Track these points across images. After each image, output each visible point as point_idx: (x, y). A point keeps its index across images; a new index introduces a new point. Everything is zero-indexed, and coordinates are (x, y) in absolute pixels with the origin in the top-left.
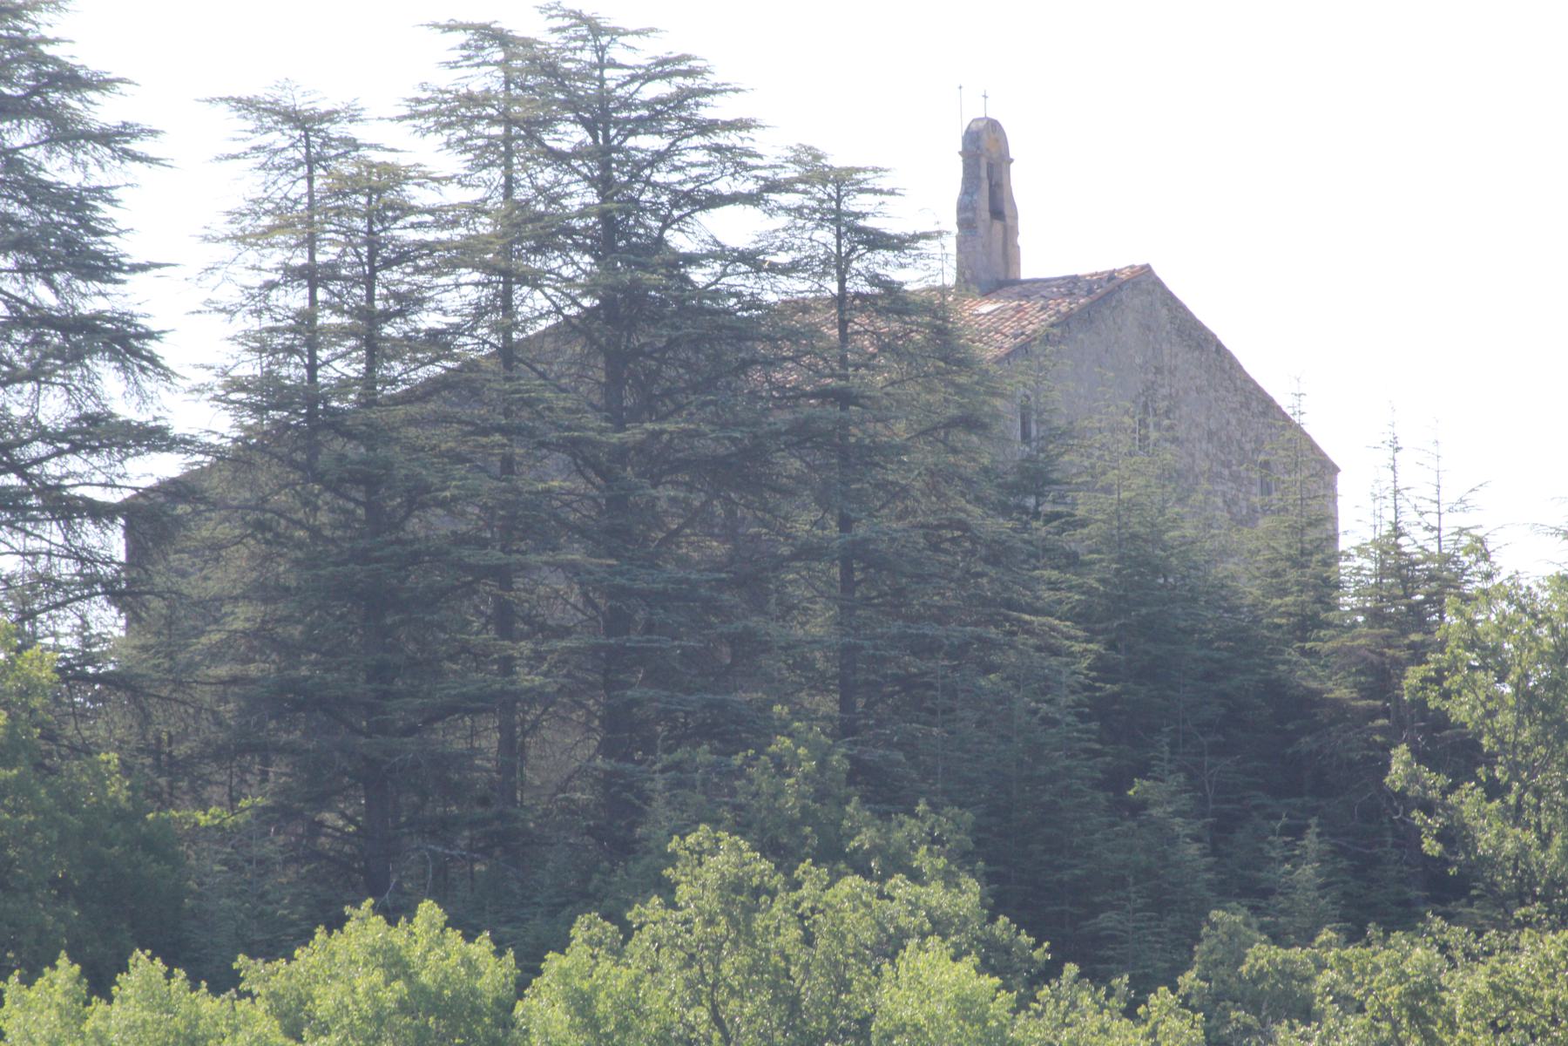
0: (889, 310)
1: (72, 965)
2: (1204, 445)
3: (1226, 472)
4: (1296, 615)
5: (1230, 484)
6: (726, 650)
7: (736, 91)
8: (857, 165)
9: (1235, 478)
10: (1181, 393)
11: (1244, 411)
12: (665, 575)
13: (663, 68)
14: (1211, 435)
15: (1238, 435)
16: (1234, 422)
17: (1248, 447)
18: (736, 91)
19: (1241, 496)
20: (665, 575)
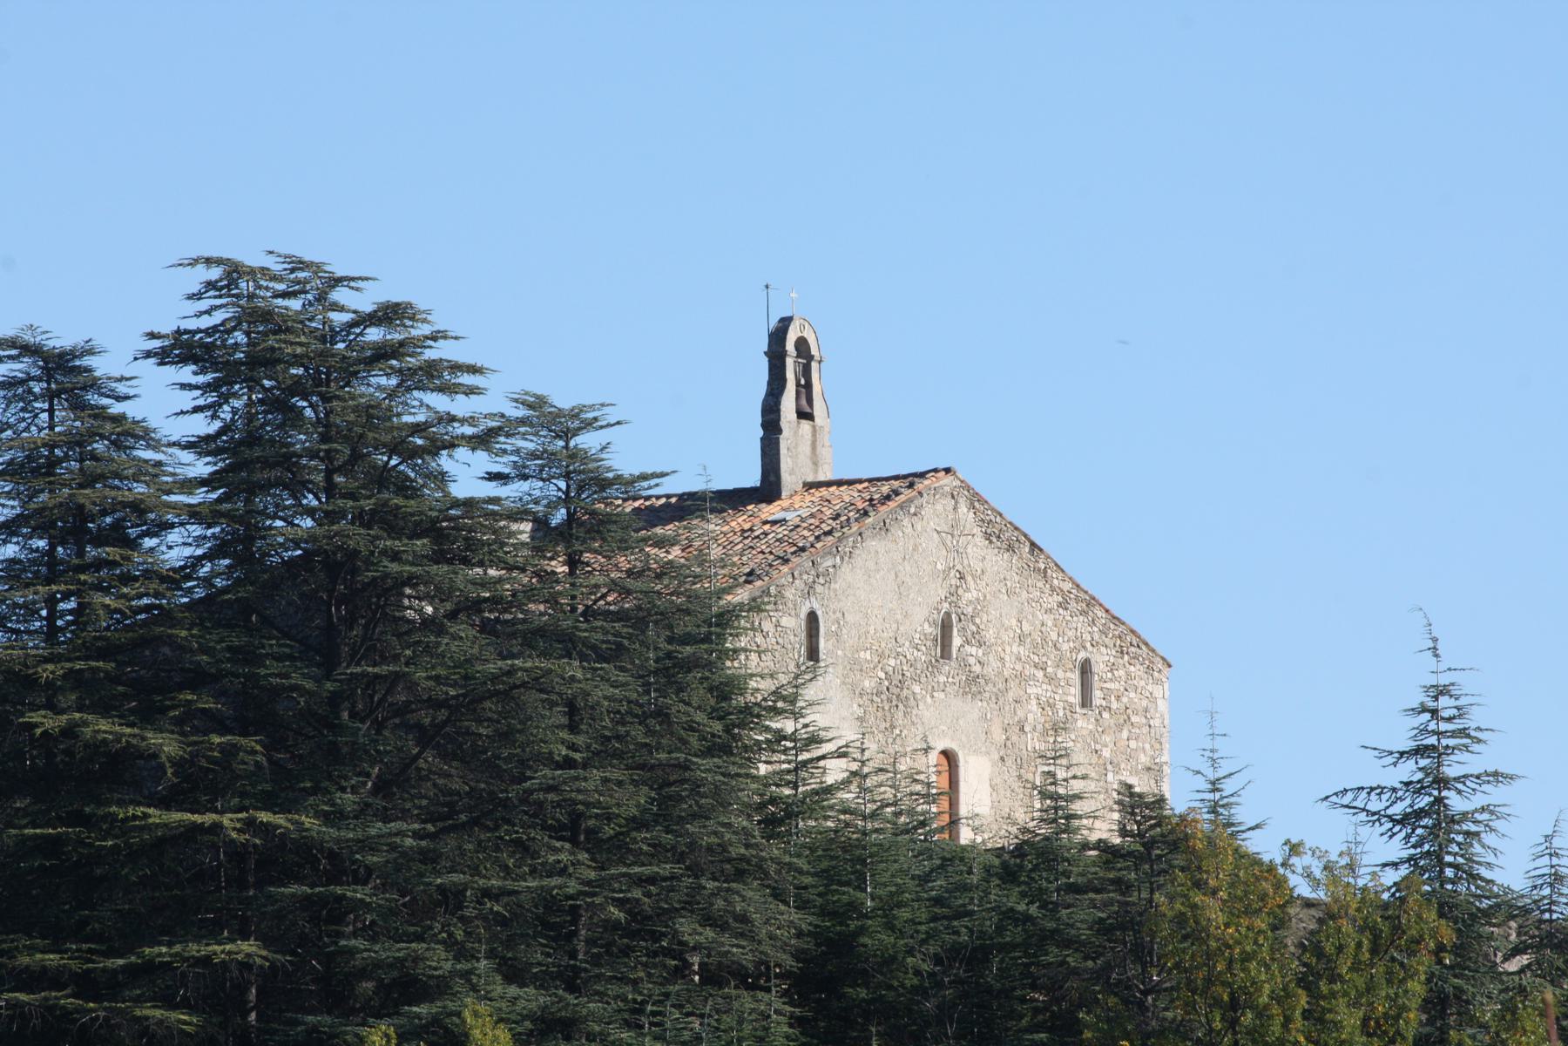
0: (194, 566)
1: (1132, 802)
2: (1015, 649)
3: (1040, 674)
4: (1209, 801)
5: (1044, 687)
6: (284, 1007)
7: (456, 338)
8: (588, 402)
9: (1050, 679)
10: (988, 597)
11: (1061, 611)
12: (625, 762)
13: (390, 314)
14: (1021, 639)
15: (1054, 636)
16: (1050, 623)
17: (1065, 647)
18: (456, 338)
19: (1057, 697)
20: (625, 762)
